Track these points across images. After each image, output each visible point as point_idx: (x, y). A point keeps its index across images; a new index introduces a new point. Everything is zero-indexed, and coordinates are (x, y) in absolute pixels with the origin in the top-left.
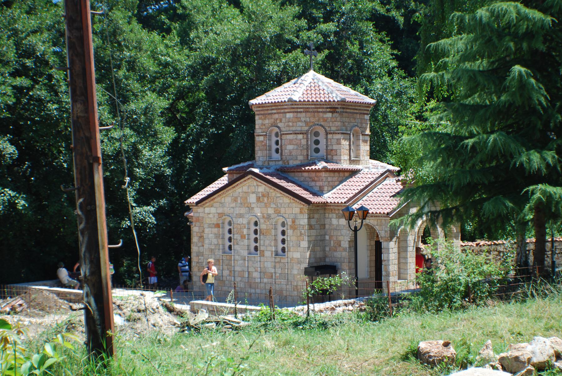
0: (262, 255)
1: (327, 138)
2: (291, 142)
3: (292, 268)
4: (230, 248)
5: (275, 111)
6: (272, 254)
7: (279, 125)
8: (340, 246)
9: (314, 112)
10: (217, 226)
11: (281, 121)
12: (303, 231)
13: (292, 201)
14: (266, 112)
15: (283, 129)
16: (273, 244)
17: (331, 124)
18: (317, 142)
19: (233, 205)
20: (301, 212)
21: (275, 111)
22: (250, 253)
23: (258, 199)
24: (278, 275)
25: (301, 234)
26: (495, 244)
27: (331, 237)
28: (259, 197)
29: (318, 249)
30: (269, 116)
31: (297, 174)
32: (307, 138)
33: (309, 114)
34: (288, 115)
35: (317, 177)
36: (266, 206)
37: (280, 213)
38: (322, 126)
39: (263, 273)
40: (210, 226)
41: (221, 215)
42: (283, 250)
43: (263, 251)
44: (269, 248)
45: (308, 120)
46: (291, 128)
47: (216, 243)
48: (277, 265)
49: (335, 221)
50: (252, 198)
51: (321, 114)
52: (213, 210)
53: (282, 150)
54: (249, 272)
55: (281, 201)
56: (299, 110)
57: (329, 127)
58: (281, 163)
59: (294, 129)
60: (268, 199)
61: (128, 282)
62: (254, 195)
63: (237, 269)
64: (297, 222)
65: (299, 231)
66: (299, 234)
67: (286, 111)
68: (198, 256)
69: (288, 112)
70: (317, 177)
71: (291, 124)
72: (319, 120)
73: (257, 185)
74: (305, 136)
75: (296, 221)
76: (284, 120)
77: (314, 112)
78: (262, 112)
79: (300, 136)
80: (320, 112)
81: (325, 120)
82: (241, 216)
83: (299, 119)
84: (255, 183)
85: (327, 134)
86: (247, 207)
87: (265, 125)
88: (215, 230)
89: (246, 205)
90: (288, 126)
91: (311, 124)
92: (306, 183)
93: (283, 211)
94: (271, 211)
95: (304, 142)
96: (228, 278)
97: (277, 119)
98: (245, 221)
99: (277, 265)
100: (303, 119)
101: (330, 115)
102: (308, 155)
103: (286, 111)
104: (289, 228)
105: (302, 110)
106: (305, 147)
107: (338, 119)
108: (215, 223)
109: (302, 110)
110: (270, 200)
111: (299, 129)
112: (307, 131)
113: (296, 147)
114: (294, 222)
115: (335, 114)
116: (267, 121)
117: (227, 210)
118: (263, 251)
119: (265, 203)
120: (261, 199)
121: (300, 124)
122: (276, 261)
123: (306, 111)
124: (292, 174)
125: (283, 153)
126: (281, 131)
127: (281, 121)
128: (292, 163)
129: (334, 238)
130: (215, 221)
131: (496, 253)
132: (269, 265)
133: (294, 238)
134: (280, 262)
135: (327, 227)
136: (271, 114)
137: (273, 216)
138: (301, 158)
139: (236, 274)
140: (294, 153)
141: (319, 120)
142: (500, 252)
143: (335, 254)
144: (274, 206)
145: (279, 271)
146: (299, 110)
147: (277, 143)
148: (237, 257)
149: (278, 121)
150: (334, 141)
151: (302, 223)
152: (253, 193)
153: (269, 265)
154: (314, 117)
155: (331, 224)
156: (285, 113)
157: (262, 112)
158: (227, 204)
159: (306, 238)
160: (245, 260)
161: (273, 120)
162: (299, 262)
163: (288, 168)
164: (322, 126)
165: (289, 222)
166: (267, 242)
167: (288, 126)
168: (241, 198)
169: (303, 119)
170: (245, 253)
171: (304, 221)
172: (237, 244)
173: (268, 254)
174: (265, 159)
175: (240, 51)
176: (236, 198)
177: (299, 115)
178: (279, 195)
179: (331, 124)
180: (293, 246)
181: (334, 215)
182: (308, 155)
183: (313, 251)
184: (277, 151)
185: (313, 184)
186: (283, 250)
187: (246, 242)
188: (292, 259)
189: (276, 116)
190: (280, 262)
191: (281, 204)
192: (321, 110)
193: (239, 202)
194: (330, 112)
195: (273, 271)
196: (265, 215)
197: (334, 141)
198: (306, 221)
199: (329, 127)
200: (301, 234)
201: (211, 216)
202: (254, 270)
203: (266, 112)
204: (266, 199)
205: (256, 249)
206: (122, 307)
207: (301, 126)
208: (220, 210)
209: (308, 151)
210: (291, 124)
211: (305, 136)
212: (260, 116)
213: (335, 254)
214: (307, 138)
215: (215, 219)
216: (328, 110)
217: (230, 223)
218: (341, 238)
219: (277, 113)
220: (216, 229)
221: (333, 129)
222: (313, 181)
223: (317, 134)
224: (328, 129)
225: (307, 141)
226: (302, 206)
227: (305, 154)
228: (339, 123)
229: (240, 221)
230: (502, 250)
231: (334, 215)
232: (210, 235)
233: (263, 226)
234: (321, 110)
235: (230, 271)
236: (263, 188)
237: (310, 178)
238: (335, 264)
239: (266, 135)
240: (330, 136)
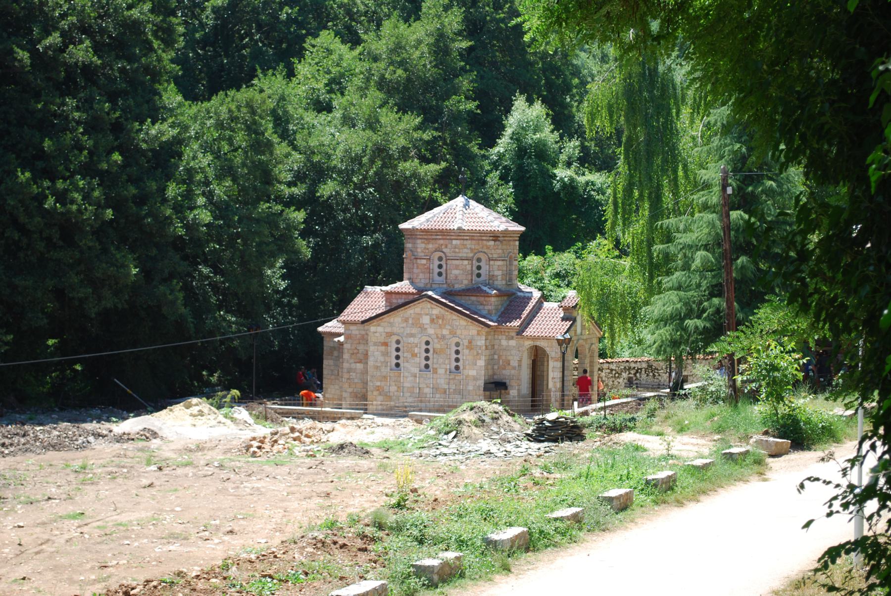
0: (435, 371)
2: (457, 267)
3: (468, 384)
4: (398, 365)
6: (446, 372)
7: (444, 250)
8: (509, 364)
9: (479, 240)
10: (386, 344)
11: (446, 247)
12: (480, 351)
13: (469, 324)
14: (430, 237)
15: (448, 254)
16: (447, 362)
17: (493, 251)
18: (479, 268)
19: (404, 325)
20: (478, 334)
21: (440, 237)
22: (420, 371)
23: (432, 321)
24: (451, 390)
25: (478, 354)
26: (607, 362)
27: (499, 357)
28: (433, 319)
29: (490, 367)
31: (463, 297)
32: (472, 264)
33: (474, 242)
34: (454, 242)
35: (486, 301)
36: (441, 327)
37: (455, 333)
38: (485, 253)
39: (436, 389)
40: (375, 344)
41: (390, 335)
42: (457, 368)
43: (436, 369)
44: (444, 366)
45: (473, 247)
46: (457, 255)
47: (382, 360)
48: (452, 382)
49: (504, 343)
50: (426, 320)
51: (485, 242)
52: (380, 329)
53: (446, 274)
54: (419, 388)
55: (458, 324)
56: (465, 238)
57: (492, 254)
58: (445, 286)
59: (460, 255)
61: (149, 409)
63: (407, 385)
64: (474, 343)
66: (475, 354)
67: (453, 237)
68: (349, 372)
70: (486, 301)
72: (482, 247)
73: (432, 308)
74: (470, 262)
75: (473, 342)
76: (449, 246)
77: (479, 240)
78: (426, 237)
79: (466, 262)
80: (482, 240)
81: (488, 248)
82: (412, 335)
83: (465, 246)
84: (429, 305)
85: (447, 260)
88: (383, 348)
89: (418, 326)
90: (455, 252)
91: (476, 251)
92: (474, 306)
93: (459, 332)
94: (445, 332)
95: (469, 267)
96: (396, 393)
97: (442, 245)
98: (416, 340)
99: (452, 382)
100: (469, 246)
101: (492, 243)
102: (472, 280)
103: (453, 237)
104: (465, 347)
105: (468, 238)
106: (470, 272)
107: (500, 247)
108: (383, 341)
109: (468, 238)
111: (465, 255)
112: (473, 257)
113: (461, 272)
114: (470, 342)
115: (497, 243)
116: (430, 246)
117: (395, 330)
118: (436, 369)
120: (435, 321)
121: (465, 250)
122: (451, 377)
123: (472, 239)
124: (459, 298)
125: (448, 277)
126: (446, 256)
127: (446, 247)
128: (458, 287)
129: (504, 358)
130: (382, 339)
131: (609, 371)
132: (442, 382)
133: (470, 358)
134: (454, 379)
135: (496, 347)
137: (447, 337)
138: (465, 282)
139: (405, 389)
140: (460, 278)
141: (482, 247)
142: (612, 370)
143: (504, 372)
144: (449, 327)
145: (453, 387)
146: (465, 238)
147: (440, 266)
148: (406, 374)
150: (495, 267)
151: (479, 343)
152: (427, 314)
153: (442, 382)
154: (479, 245)
155: (500, 345)
156: (452, 239)
157: (426, 237)
158: (397, 324)
159: (483, 358)
160: (416, 377)
161: (437, 245)
162: (475, 379)
163: (455, 291)
164: (485, 253)
165: (466, 343)
166: (441, 361)
167: (455, 252)
168: (413, 319)
169: (469, 246)
170: (416, 370)
171: (481, 342)
172: (407, 362)
173: (441, 371)
174: (427, 281)
177: (465, 242)
178: (454, 317)
179: (493, 251)
180: (469, 364)
181: (504, 337)
182: (472, 280)
183: (486, 369)
184: (440, 274)
185: (481, 307)
186: (457, 368)
187: (417, 360)
188: (467, 376)
189: (442, 242)
190: (454, 379)
191: (457, 326)
192: (484, 238)
193: (410, 322)
194: (493, 240)
195: (446, 387)
196: (440, 336)
197: (495, 267)
198: (483, 342)
199: (492, 254)
200: (478, 354)
201: (377, 334)
202: (425, 386)
203: (430, 237)
204: (440, 321)
205: (427, 366)
207: (466, 253)
208: (388, 330)
209: (472, 276)
210: (457, 250)
211: (470, 262)
213: (504, 372)
214: (472, 264)
216: (491, 238)
217: (398, 342)
218: (510, 358)
219: (444, 239)
220: (384, 347)
221: (495, 256)
223: (479, 260)
224: (490, 256)
225: (472, 267)
226: (480, 329)
227: (470, 278)
228: (500, 251)
229: (411, 340)
230: (614, 368)
231: (504, 337)
232: (376, 353)
233: (435, 345)
234: (484, 238)
235: (398, 387)
236: (437, 310)
237: (478, 302)
238: (504, 381)
239: (429, 259)
240: (492, 263)
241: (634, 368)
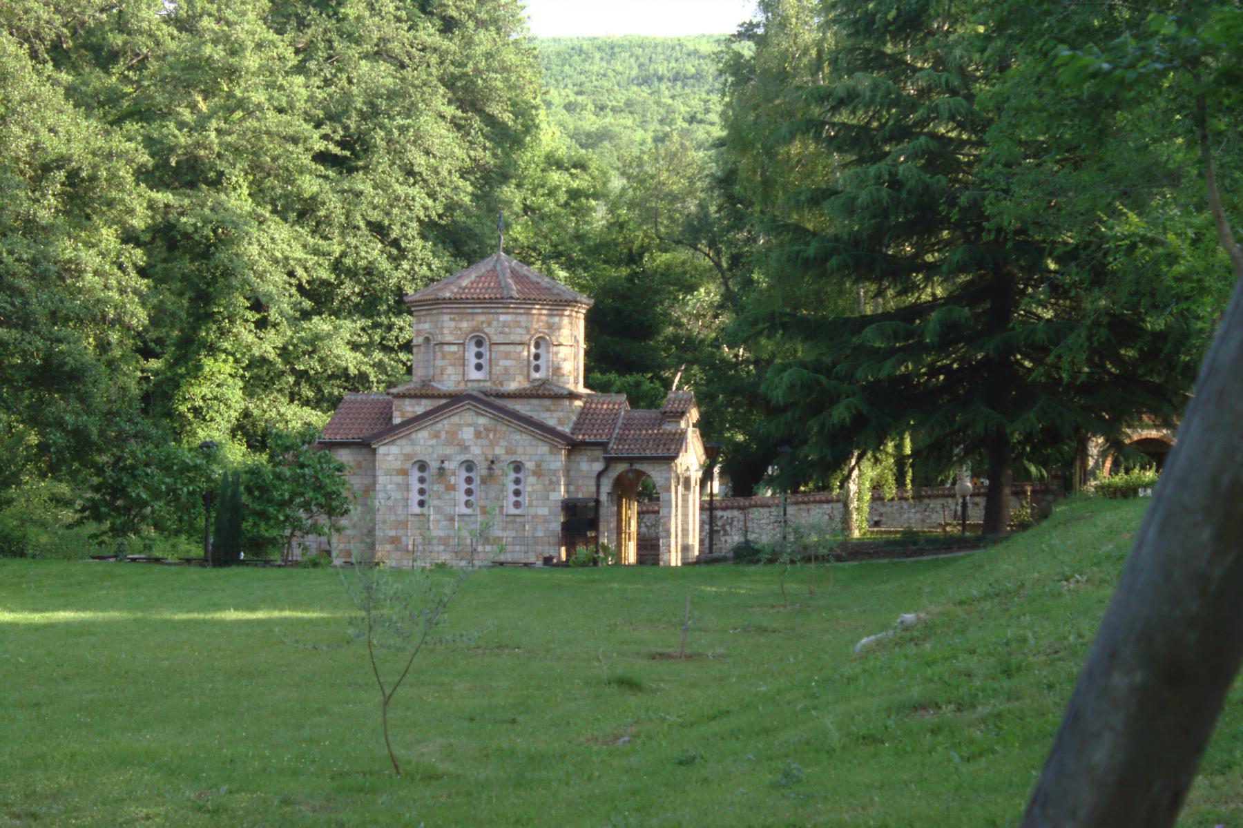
1: (490, 351)
5: (480, 311)
7: (487, 330)
19: (434, 442)
30: (470, 317)
40: (388, 473)
52: (394, 449)
60: (495, 435)
62: (471, 429)
64: (544, 466)
65: (547, 478)
66: (547, 483)
69: (502, 313)
71: (507, 330)
76: (495, 323)
86: (458, 445)
87: (460, 329)
94: (499, 451)
100: (523, 324)
106: (525, 363)
110: (498, 436)
119: (490, 440)
121: (519, 330)
130: (398, 465)
136: (473, 314)
149: (484, 325)
152: (470, 425)
168: (447, 433)
169: (523, 324)
175: (292, 216)
176: (439, 432)
177: (519, 318)
189: (482, 318)
201: (390, 458)
206: (1014, 661)
210: (507, 330)
212: (452, 316)
215: (399, 463)
219: (483, 313)
222: (547, 410)
241: (722, 517)
